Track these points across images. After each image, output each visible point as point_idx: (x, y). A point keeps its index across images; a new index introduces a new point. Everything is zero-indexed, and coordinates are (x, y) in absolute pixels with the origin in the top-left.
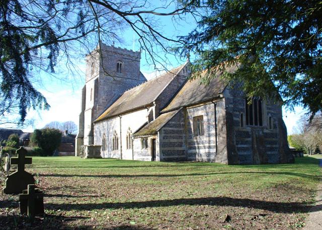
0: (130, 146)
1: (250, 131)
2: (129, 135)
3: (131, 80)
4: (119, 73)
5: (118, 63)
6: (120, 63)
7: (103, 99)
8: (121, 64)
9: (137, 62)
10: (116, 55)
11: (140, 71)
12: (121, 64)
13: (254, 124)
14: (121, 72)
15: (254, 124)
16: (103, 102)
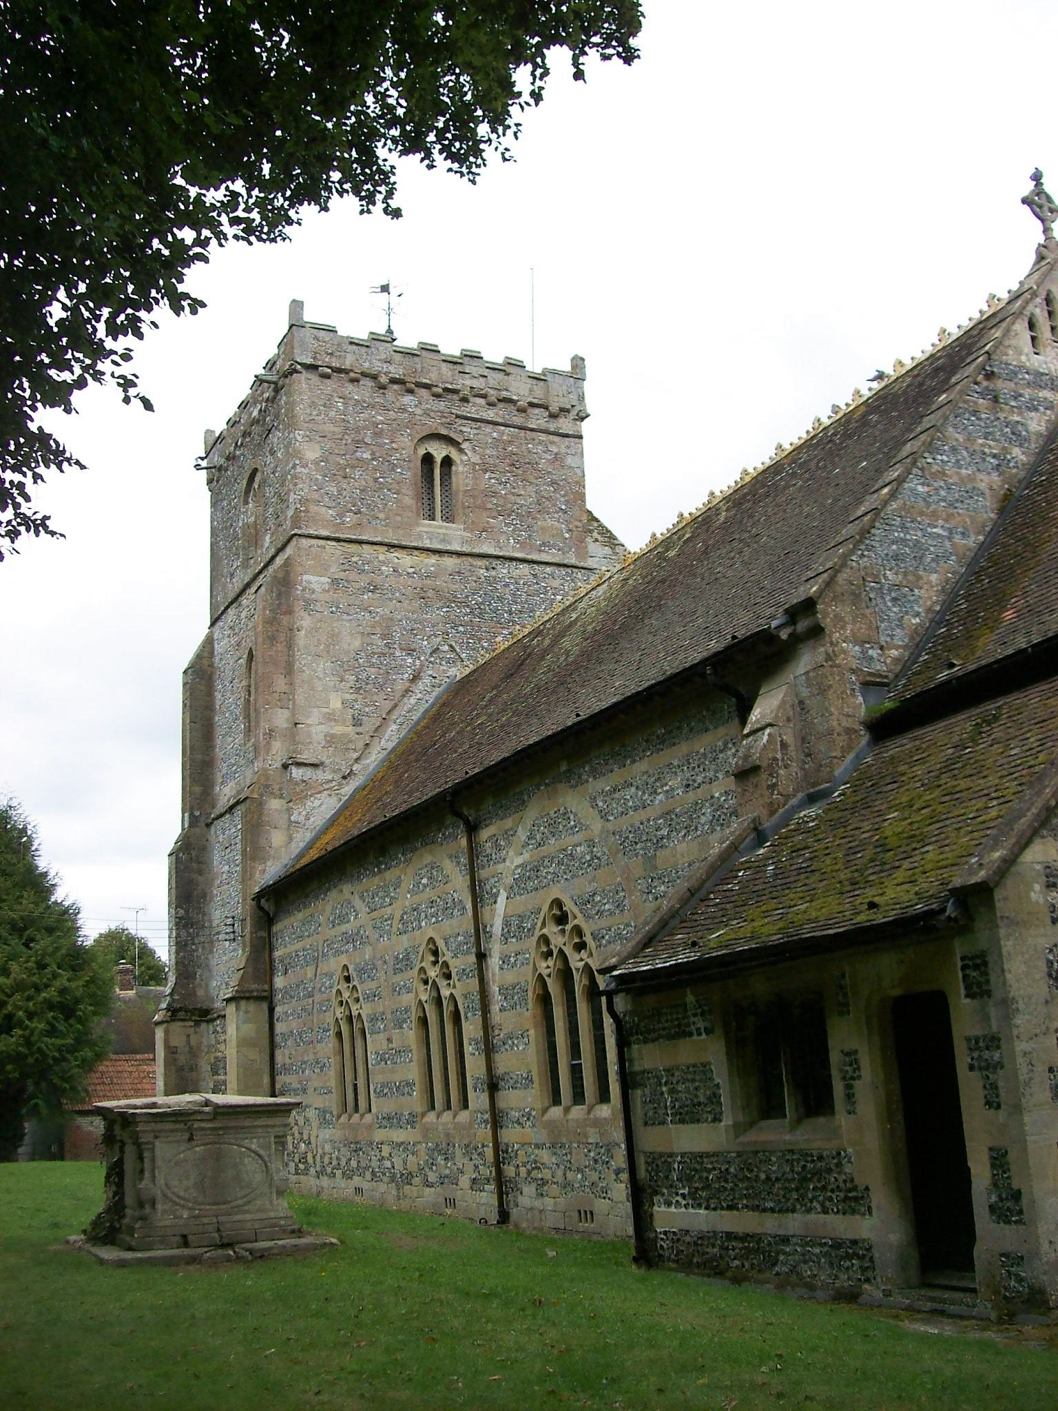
0: (576, 1071)
1: (178, 286)
2: (566, 975)
3: (525, 569)
4: (439, 522)
5: (428, 459)
6: (439, 452)
7: (330, 718)
8: (447, 462)
9: (561, 445)
10: (407, 399)
11: (589, 506)
12: (447, 462)
13: (438, 459)
14: (449, 518)
15: (438, 459)
16: (331, 740)
